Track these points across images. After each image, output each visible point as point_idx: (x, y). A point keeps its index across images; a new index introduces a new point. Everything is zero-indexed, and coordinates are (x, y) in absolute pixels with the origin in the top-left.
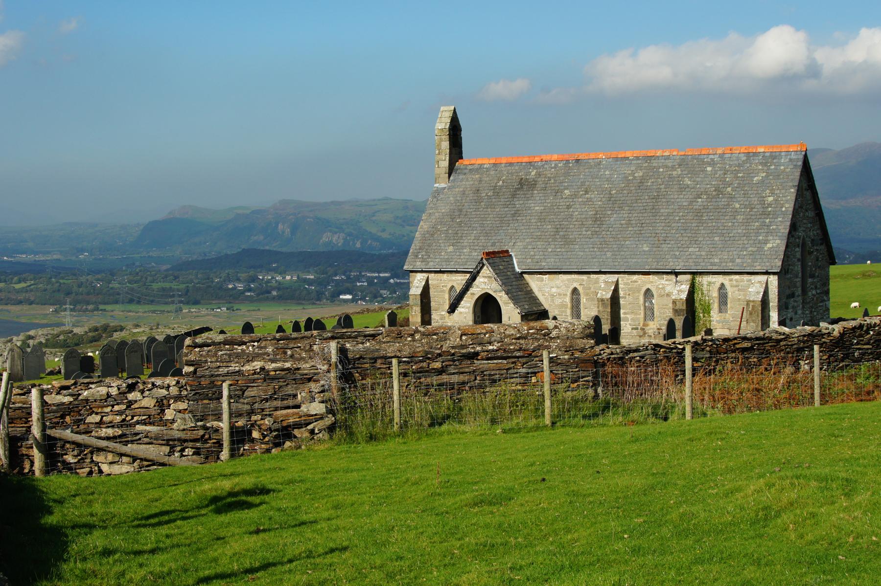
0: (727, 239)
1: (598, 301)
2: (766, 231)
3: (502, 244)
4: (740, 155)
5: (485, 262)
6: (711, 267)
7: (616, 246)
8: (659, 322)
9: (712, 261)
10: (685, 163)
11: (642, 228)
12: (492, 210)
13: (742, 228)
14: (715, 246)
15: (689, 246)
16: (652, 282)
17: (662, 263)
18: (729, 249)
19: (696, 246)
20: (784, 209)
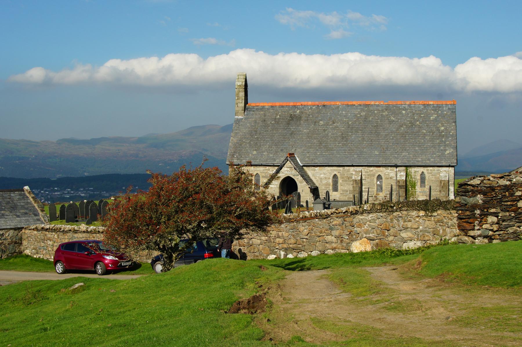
0: (423, 148)
1: (353, 181)
2: (444, 144)
3: (287, 150)
4: (420, 105)
5: (289, 159)
6: (418, 163)
7: (359, 152)
8: (386, 193)
9: (417, 160)
10: (389, 109)
11: (372, 143)
12: (277, 131)
13: (430, 143)
14: (416, 152)
15: (402, 152)
16: (382, 171)
17: (388, 161)
18: (425, 154)
19: (406, 152)
20: (451, 134)
